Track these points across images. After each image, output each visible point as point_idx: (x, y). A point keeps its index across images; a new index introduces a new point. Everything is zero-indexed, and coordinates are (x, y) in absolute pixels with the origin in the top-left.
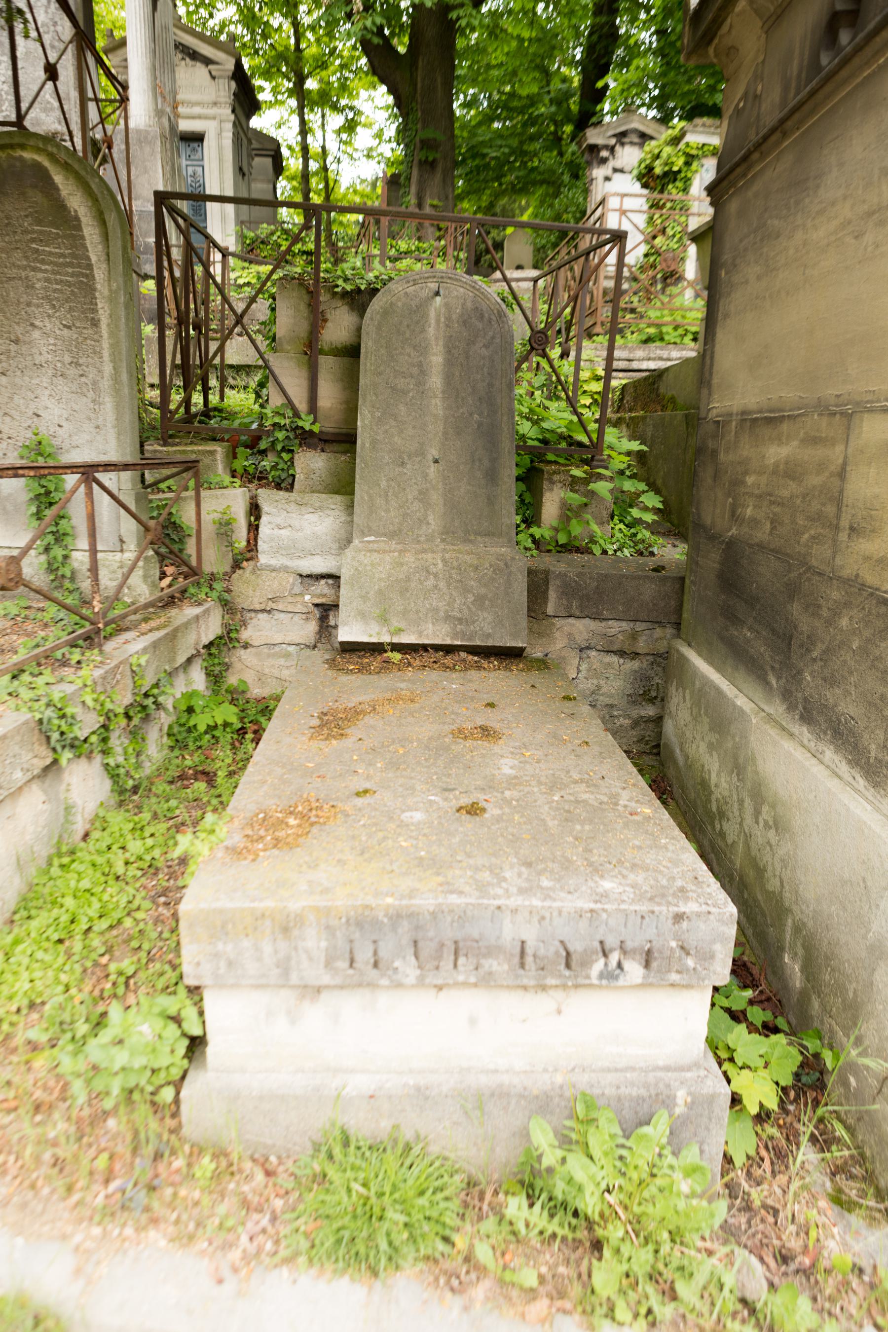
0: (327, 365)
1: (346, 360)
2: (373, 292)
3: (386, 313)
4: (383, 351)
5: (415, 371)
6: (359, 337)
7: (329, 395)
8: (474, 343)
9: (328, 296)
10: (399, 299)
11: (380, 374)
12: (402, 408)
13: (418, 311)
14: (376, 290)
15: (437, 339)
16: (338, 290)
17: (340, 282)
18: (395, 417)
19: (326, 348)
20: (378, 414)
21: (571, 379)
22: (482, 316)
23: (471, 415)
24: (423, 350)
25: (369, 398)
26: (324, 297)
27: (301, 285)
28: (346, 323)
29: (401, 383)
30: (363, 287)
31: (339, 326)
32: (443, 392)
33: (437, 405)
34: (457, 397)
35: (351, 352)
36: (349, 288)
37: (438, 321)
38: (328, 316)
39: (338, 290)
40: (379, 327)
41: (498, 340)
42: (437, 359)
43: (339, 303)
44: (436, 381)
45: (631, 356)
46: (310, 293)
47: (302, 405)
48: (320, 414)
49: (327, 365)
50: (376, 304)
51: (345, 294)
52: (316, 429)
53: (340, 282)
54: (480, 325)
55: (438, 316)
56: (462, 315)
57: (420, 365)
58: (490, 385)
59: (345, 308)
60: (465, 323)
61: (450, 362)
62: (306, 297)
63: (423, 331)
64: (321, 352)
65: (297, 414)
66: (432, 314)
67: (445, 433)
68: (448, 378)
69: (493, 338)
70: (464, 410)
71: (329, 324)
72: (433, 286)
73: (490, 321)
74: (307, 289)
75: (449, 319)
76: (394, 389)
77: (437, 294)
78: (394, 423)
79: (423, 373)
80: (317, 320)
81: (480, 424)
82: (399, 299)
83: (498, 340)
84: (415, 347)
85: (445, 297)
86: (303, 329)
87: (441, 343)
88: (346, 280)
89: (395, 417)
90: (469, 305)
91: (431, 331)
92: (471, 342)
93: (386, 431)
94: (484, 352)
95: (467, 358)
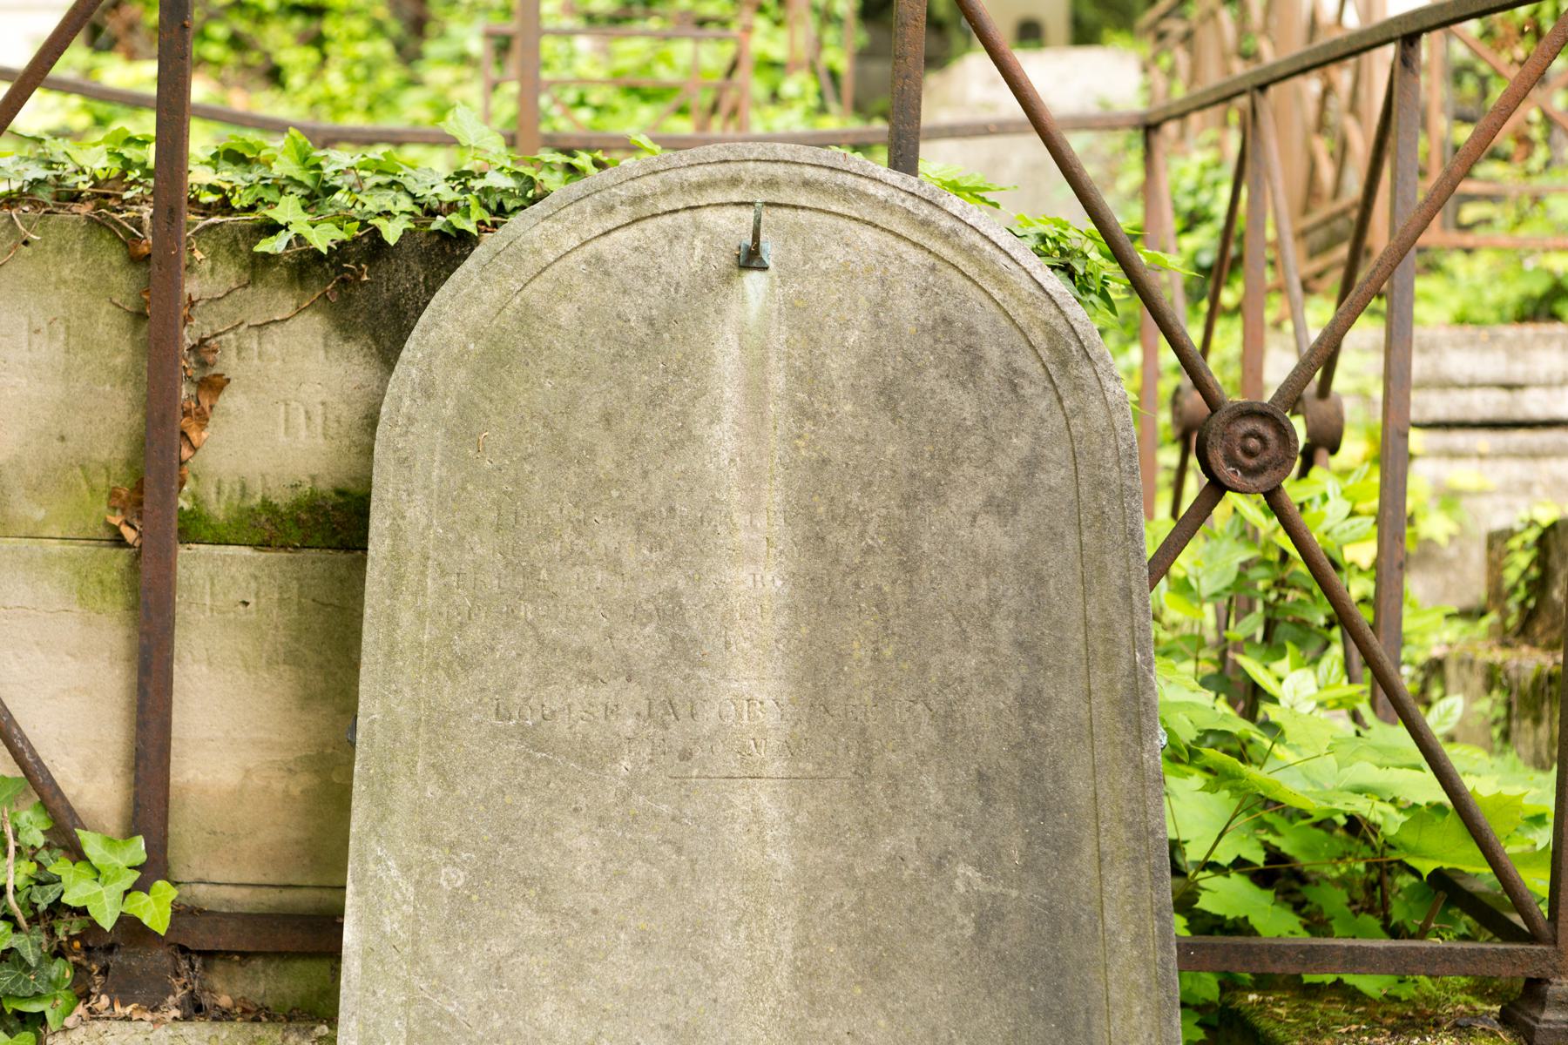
0: (223, 591)
1: (314, 562)
2: (446, 249)
3: (497, 357)
4: (483, 547)
5: (645, 641)
6: (368, 452)
7: (229, 732)
8: (937, 492)
9: (230, 273)
10: (563, 290)
11: (466, 663)
12: (580, 840)
13: (654, 351)
14: (455, 246)
15: (752, 475)
16: (274, 245)
17: (288, 210)
18: (540, 888)
19: (218, 509)
20: (453, 878)
21: (1362, 553)
22: (972, 360)
23: (939, 864)
24: (677, 530)
25: (404, 791)
26: (206, 278)
27: (97, 224)
28: (313, 394)
29: (573, 707)
30: (392, 232)
31: (279, 406)
32: (792, 749)
33: (760, 819)
34: (864, 771)
35: (332, 526)
36: (322, 238)
37: (756, 391)
38: (228, 363)
39: (274, 245)
40: (464, 429)
41: (1055, 476)
42: (753, 576)
43: (284, 303)
44: (751, 689)
45: (1518, 372)
46: (137, 260)
47: (94, 781)
48: (184, 828)
49: (223, 591)
50: (454, 314)
51: (306, 266)
52: (155, 911)
53: (288, 210)
54: (965, 405)
55: (757, 363)
56: (876, 355)
57: (670, 610)
58: (1032, 704)
59: (313, 326)
60: (888, 394)
61: (820, 592)
62: (123, 284)
63: (683, 438)
64: (193, 529)
65: (64, 836)
66: (727, 358)
67: (807, 973)
68: (816, 678)
69: (1032, 464)
70: (902, 839)
71: (230, 400)
72: (733, 226)
73: (1012, 380)
74: (129, 242)
75: (808, 376)
76: (535, 740)
77: (750, 259)
78: (533, 924)
79: (683, 650)
80: (172, 383)
81: (988, 917)
82: (563, 290)
83: (1055, 476)
84: (640, 524)
85: (789, 273)
86: (108, 423)
87: (773, 497)
88: (317, 195)
89: (540, 888)
90: (907, 307)
91: (724, 439)
92: (923, 491)
93: (495, 972)
94: (993, 536)
95: (909, 567)
